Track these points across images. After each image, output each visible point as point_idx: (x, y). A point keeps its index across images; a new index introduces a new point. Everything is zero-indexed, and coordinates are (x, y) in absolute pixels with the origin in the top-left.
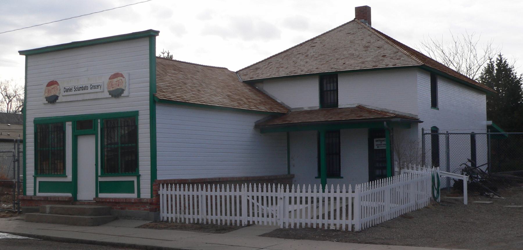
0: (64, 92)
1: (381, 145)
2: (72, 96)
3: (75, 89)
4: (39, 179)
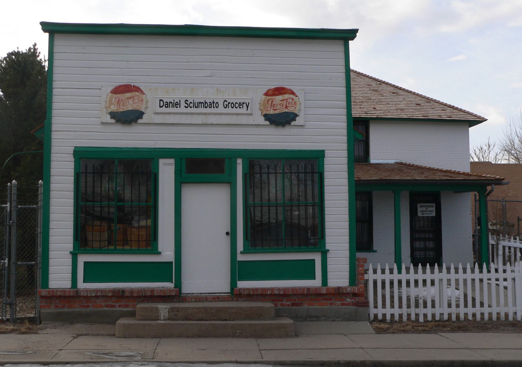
0: (160, 107)
1: (427, 211)
2: (184, 116)
3: (186, 103)
4: (82, 259)
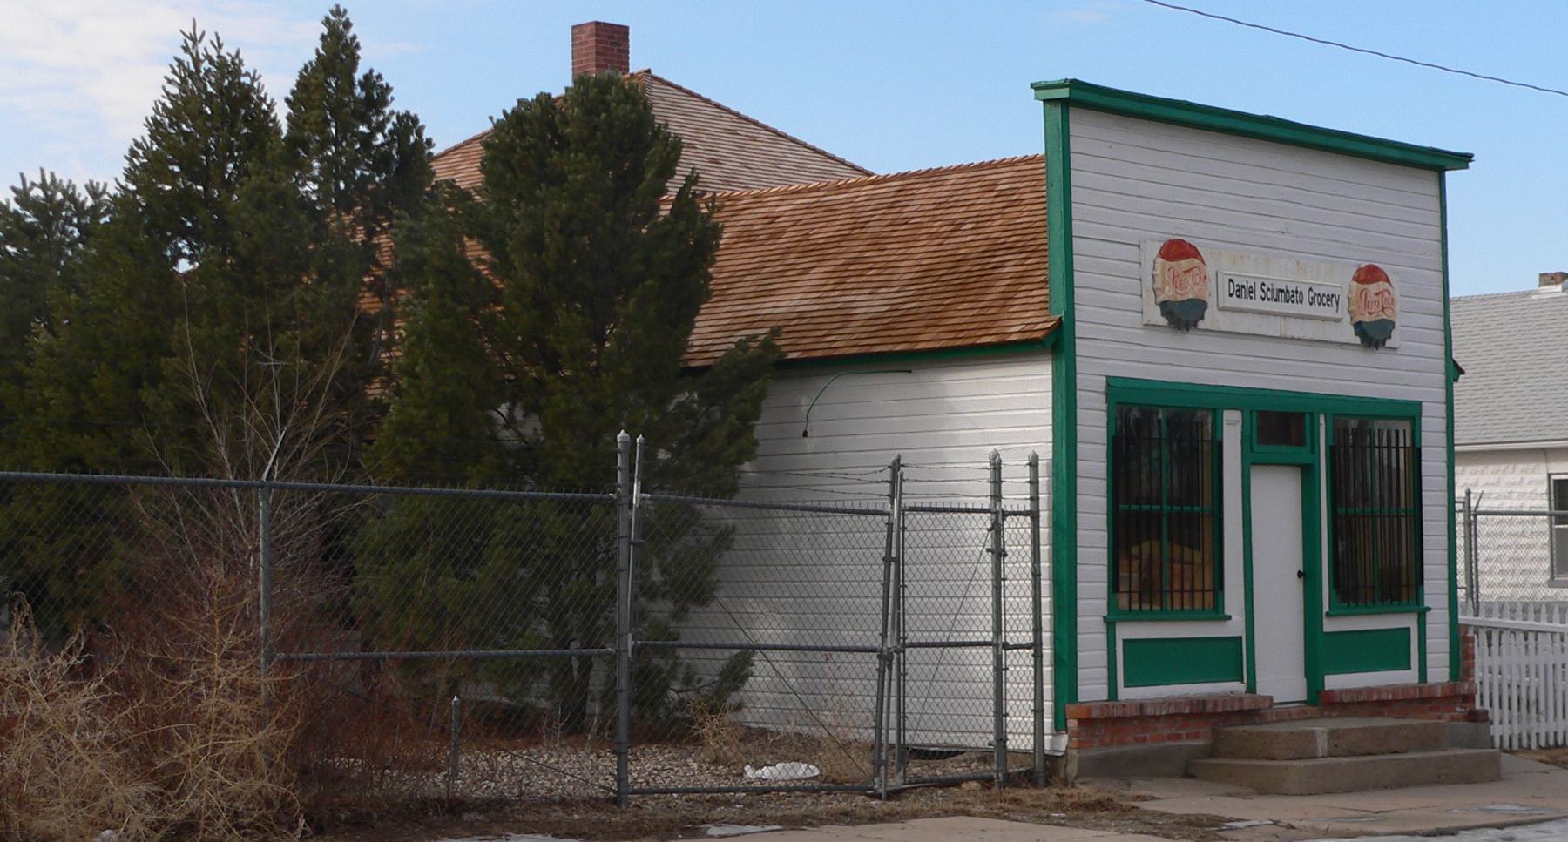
4: (1126, 632)
